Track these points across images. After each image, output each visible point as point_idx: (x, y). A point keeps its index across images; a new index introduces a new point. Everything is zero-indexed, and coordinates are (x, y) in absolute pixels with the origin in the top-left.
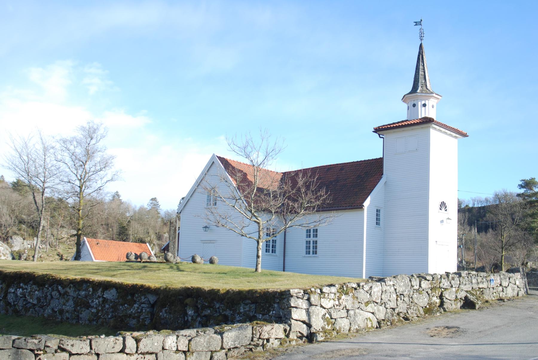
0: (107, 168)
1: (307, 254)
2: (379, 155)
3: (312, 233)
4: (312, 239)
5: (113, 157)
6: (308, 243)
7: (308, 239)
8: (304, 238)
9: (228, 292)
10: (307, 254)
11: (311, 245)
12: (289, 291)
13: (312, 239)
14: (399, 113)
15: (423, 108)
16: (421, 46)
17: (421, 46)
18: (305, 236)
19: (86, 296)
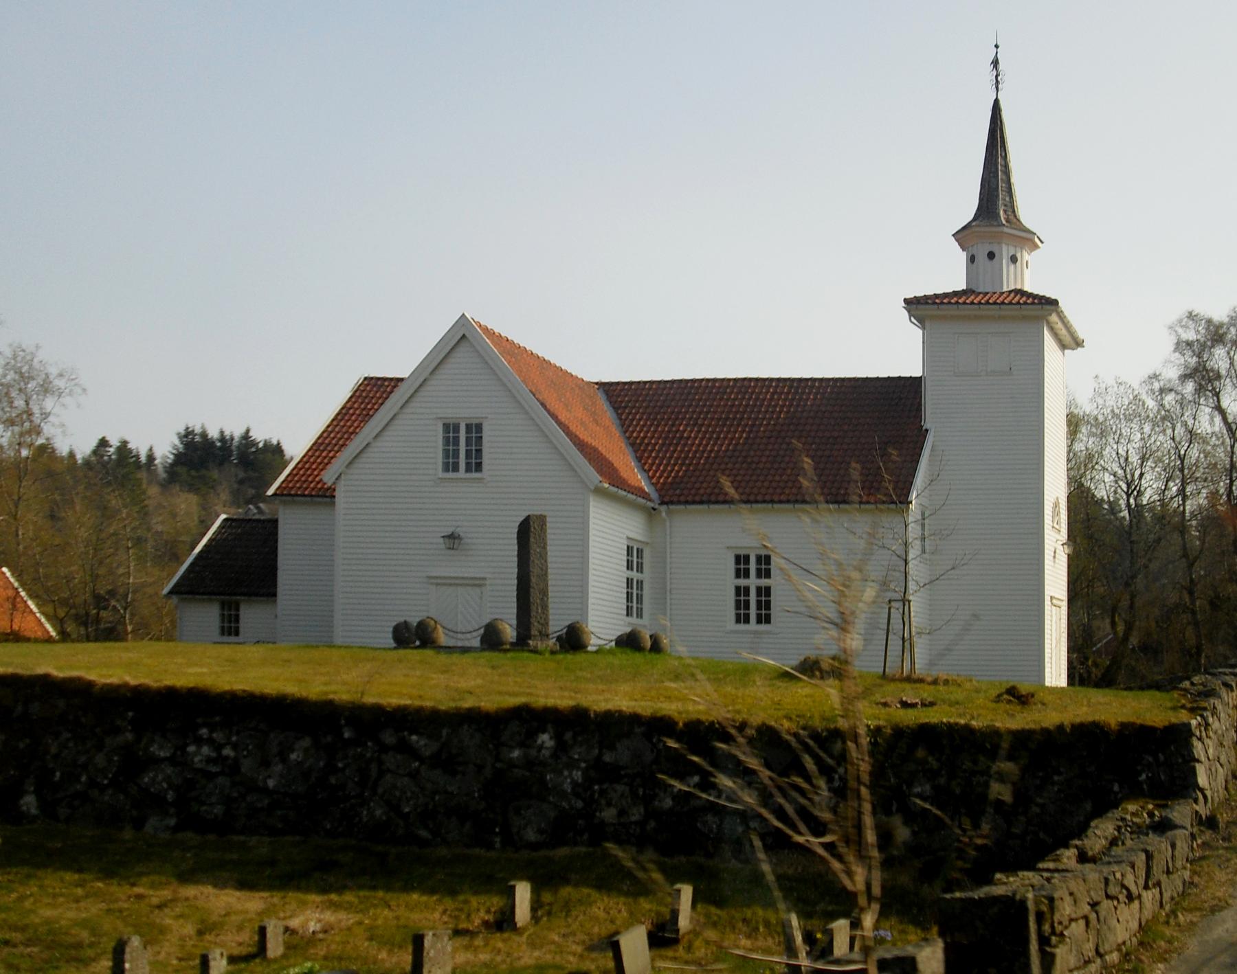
0: (24, 347)
1: (738, 621)
2: (917, 372)
3: (753, 566)
4: (753, 582)
5: (222, 432)
6: (741, 591)
7: (742, 582)
8: (730, 581)
9: (1124, 726)
10: (738, 621)
11: (753, 598)
12: (64, 636)
13: (753, 582)
14: (949, 273)
15: (1012, 267)
16: (996, 102)
17: (996, 102)
18: (732, 573)
19: (529, 764)
